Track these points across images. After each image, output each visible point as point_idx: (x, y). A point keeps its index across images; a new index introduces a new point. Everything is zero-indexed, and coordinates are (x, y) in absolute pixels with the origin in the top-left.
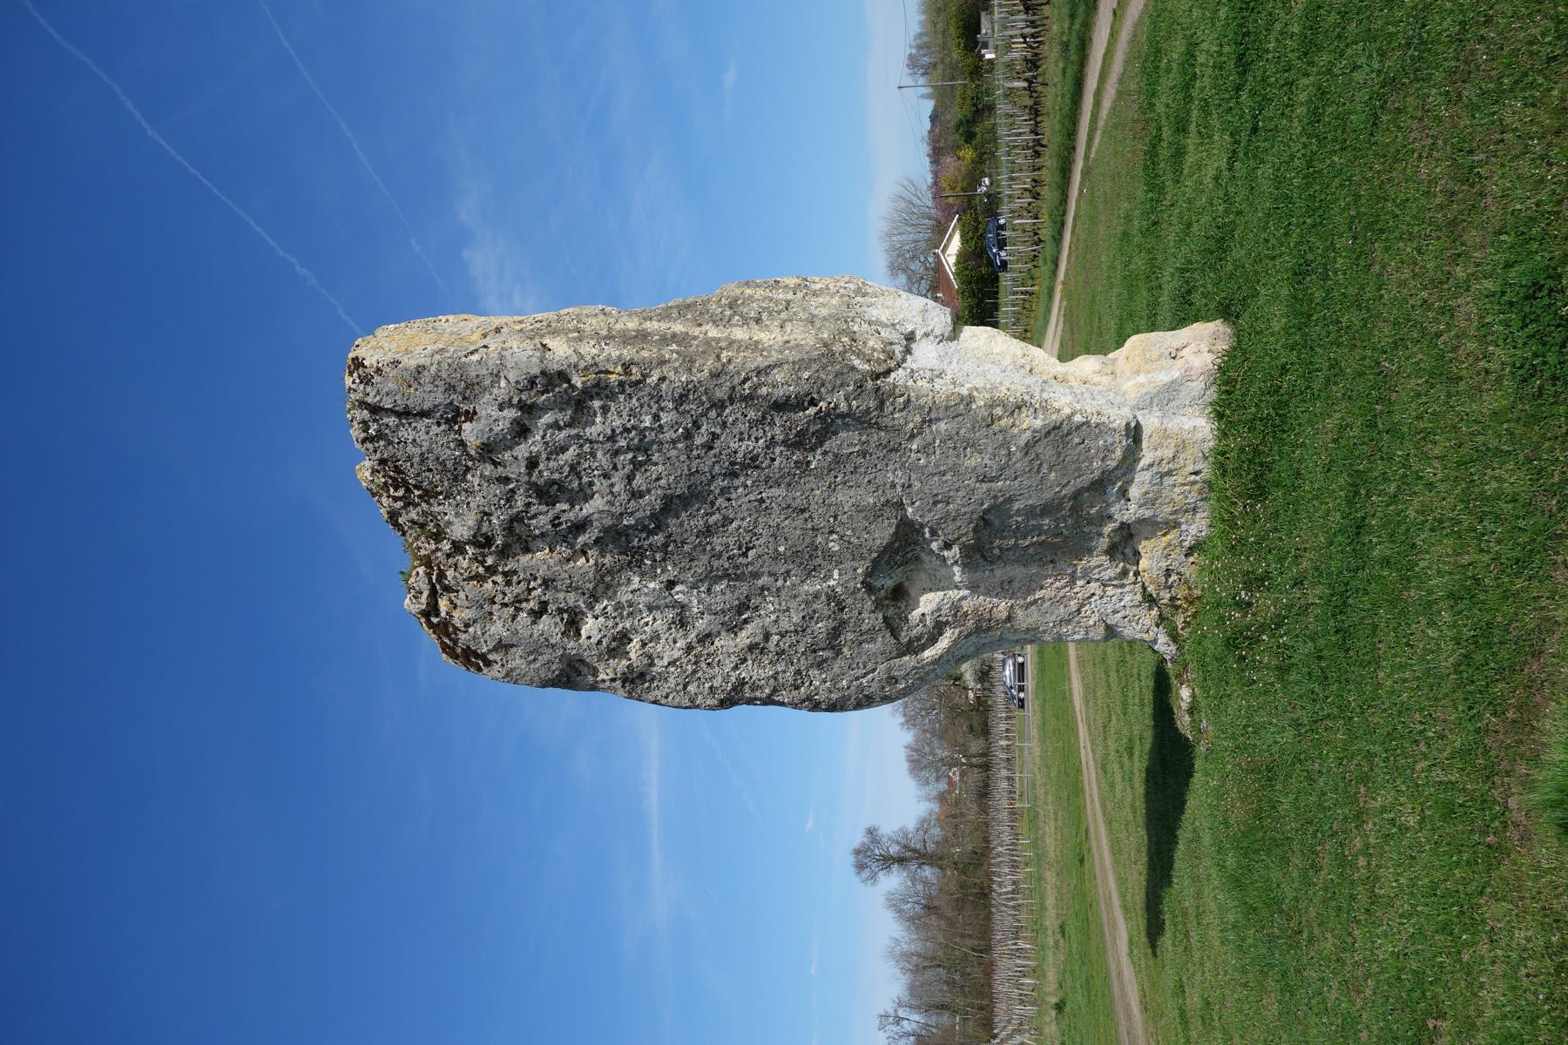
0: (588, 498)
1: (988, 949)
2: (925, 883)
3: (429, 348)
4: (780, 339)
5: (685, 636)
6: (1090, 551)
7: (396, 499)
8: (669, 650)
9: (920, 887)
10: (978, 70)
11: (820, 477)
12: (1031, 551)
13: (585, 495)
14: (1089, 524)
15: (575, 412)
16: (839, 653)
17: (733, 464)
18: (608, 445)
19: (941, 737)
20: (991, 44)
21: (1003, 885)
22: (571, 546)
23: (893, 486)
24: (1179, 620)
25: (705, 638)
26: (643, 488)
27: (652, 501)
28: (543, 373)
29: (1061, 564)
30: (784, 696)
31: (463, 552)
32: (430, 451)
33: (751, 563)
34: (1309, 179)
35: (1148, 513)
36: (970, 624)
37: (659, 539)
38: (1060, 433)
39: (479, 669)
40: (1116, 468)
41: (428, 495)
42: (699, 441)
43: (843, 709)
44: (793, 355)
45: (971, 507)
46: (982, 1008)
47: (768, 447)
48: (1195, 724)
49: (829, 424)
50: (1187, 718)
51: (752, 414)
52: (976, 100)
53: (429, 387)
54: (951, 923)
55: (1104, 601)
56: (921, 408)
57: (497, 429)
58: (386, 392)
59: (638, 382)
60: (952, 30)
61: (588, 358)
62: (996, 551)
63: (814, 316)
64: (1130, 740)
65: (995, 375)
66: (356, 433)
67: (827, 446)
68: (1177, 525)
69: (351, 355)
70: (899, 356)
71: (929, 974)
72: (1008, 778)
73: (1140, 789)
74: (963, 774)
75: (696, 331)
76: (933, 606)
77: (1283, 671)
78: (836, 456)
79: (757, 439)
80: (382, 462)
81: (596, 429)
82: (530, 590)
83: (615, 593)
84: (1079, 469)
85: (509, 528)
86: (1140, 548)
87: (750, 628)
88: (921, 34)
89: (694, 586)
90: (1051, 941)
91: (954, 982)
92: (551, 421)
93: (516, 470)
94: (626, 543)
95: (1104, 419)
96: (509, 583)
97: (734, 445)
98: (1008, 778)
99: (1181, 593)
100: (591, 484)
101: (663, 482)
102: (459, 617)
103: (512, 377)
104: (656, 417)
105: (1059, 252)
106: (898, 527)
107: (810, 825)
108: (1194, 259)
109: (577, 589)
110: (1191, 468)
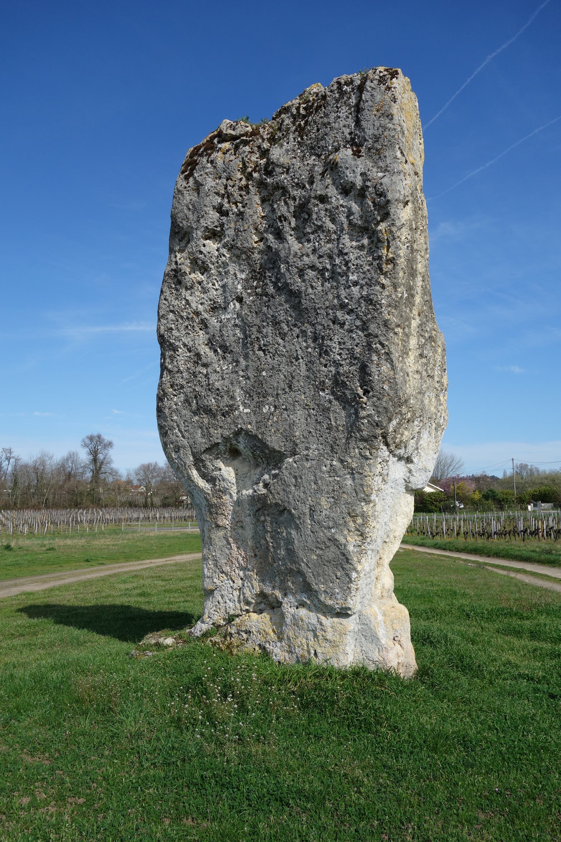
0: (299, 239)
1: (47, 507)
2: (83, 473)
3: (405, 124)
4: (410, 370)
5: (206, 311)
6: (263, 581)
7: (298, 109)
8: (196, 300)
9: (80, 470)
10: (522, 502)
11: (314, 398)
12: (263, 541)
13: (301, 237)
14: (281, 580)
15: (360, 227)
16: (195, 413)
17: (323, 338)
18: (336, 251)
19: (161, 482)
20: (536, 509)
21: (84, 515)
22: (266, 231)
23: (307, 449)
24: (217, 639)
25: (204, 325)
26: (306, 277)
27: (297, 283)
28: (388, 202)
29: (254, 561)
30: (167, 378)
31: (261, 157)
32: (332, 129)
34: (535, 749)
35: (288, 621)
36: (214, 501)
37: (271, 289)
38: (344, 563)
39: (183, 172)
40: (319, 600)
41: (301, 131)
42: (339, 314)
43: (159, 417)
44: (399, 377)
45: (293, 502)
46: (15, 504)
47: (334, 362)
48: (148, 647)
49: (351, 404)
50: (153, 642)
51: (358, 350)
52: (506, 501)
53: (377, 124)
54: (61, 487)
55: (228, 592)
56: (362, 467)
57: (348, 172)
58: (374, 95)
59: (381, 269)
60: (544, 488)
61: (398, 234)
62: (262, 518)
63: (424, 394)
64: (149, 594)
65: (383, 518)
66: (344, 78)
67: (335, 403)
68: (280, 639)
69: (399, 70)
70: (398, 452)
71: (33, 476)
72: (138, 518)
73: (118, 602)
74: (142, 493)
75: (415, 312)
76: (226, 475)
77: (177, 722)
78: (328, 409)
79: (340, 354)
80: (324, 97)
81: (347, 242)
82: (236, 203)
83: (235, 262)
84: (319, 575)
86: (264, 614)
87: (211, 354)
88: (538, 471)
89: (239, 316)
90: (46, 542)
91: (29, 489)
92: (354, 210)
93: (319, 189)
94: (268, 268)
95: (353, 593)
96: (240, 189)
97: (336, 338)
98: (138, 518)
99: (235, 641)
100: (309, 241)
101: (310, 290)
102: (218, 156)
103: (386, 180)
104: (356, 284)
105: (428, 547)
106: (279, 452)
107: (116, 412)
108: (454, 647)
109: (237, 235)
110: (319, 651)
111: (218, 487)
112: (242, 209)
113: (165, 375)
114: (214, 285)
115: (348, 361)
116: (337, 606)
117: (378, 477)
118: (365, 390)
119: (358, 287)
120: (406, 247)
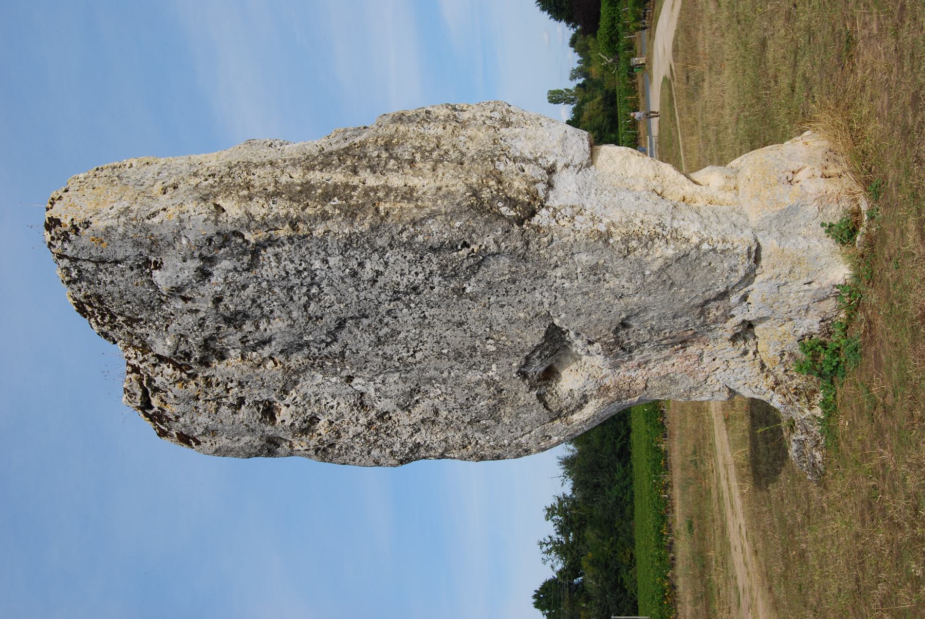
16: (498, 421)
28: (218, 234)
33: (420, 362)
37: (336, 348)
44: (443, 205)
53: (119, 243)
59: (305, 236)
79: (417, 274)
82: (228, 390)
85: (206, 345)
87: (422, 405)
93: (205, 306)
104: (325, 261)
111: (595, 392)
112: (235, 383)
113: (452, 455)
114: (332, 407)
115: (425, 266)
116: (747, 265)
117: (576, 223)
118: (462, 247)
119: (329, 258)
120: (274, 206)
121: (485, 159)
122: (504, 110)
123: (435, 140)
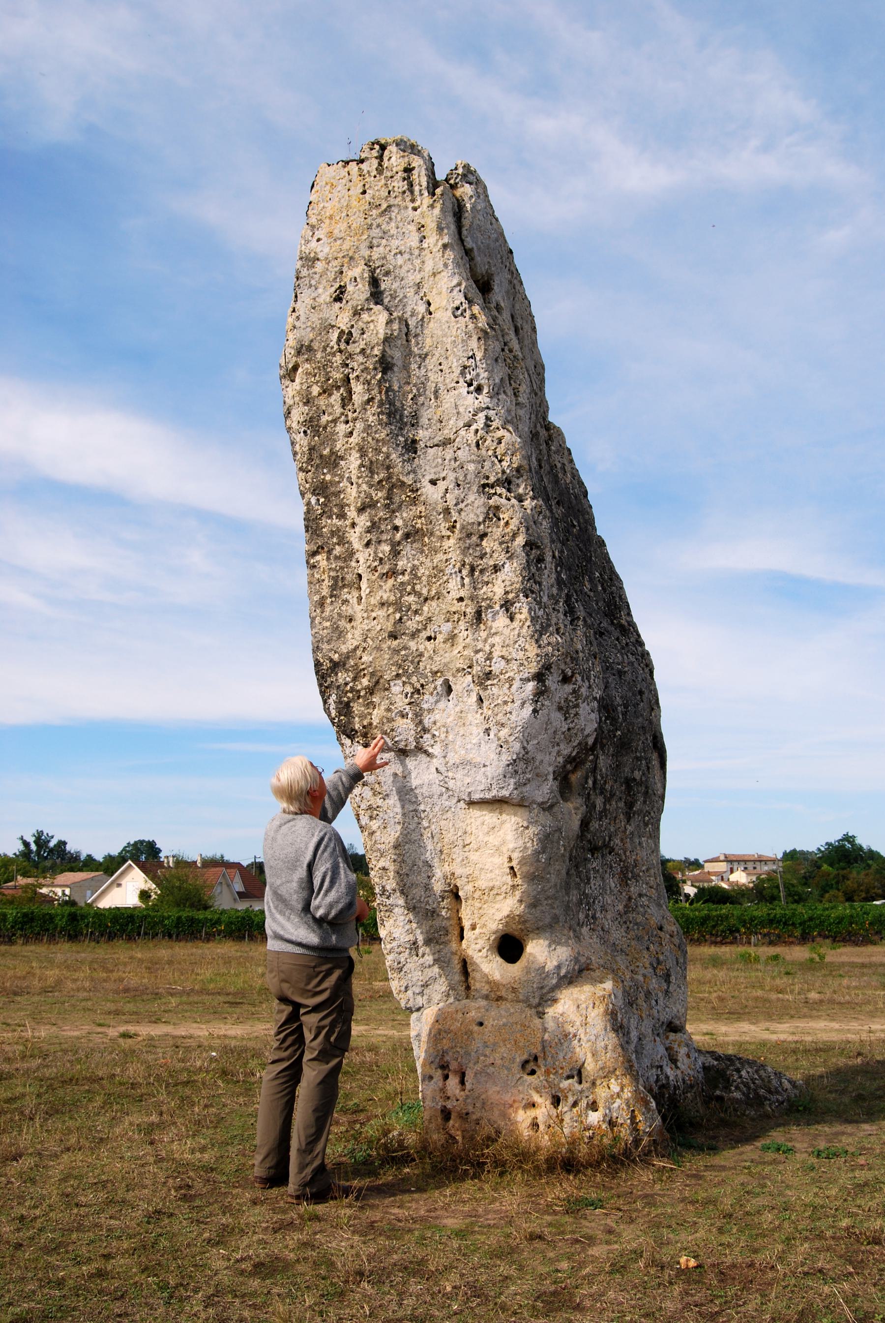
121: (400, 667)
122: (511, 674)
123: (433, 593)
